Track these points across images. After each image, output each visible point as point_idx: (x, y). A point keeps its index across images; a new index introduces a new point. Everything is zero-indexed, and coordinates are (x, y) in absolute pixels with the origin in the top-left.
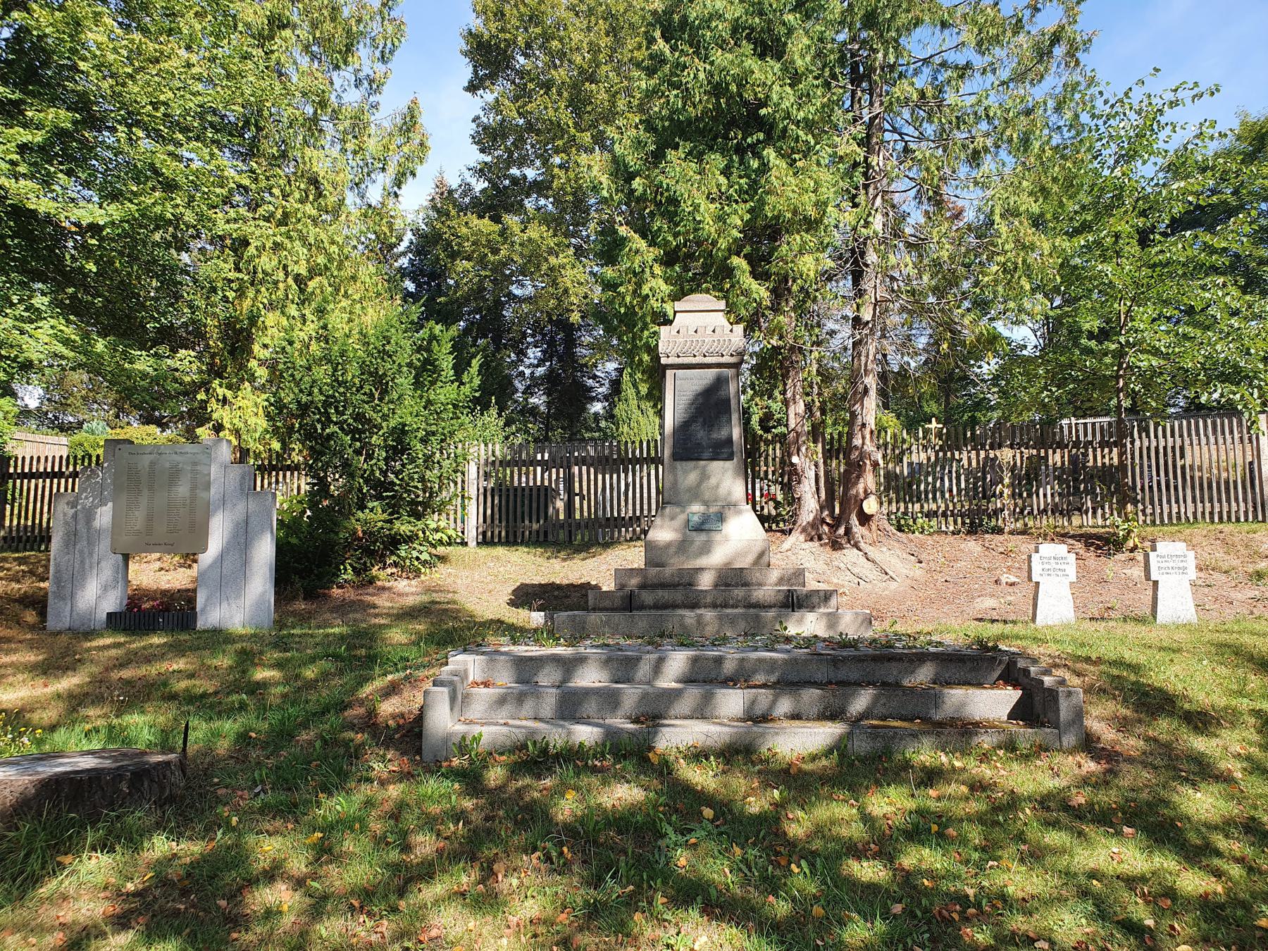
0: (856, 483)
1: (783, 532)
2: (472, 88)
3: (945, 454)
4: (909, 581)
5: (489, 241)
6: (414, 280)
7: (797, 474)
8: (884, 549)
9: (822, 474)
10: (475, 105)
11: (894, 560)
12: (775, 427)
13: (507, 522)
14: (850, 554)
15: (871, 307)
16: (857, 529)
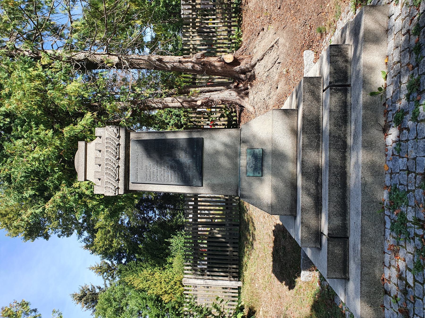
0: (214, 66)
1: (241, 111)
2: (47, 237)
3: (197, 26)
4: (279, 32)
5: (105, 234)
6: (122, 259)
7: (208, 102)
8: (255, 50)
9: (207, 89)
10: (53, 237)
11: (263, 44)
12: (181, 122)
13: (227, 264)
14: (259, 70)
15: (110, 56)
16: (243, 65)
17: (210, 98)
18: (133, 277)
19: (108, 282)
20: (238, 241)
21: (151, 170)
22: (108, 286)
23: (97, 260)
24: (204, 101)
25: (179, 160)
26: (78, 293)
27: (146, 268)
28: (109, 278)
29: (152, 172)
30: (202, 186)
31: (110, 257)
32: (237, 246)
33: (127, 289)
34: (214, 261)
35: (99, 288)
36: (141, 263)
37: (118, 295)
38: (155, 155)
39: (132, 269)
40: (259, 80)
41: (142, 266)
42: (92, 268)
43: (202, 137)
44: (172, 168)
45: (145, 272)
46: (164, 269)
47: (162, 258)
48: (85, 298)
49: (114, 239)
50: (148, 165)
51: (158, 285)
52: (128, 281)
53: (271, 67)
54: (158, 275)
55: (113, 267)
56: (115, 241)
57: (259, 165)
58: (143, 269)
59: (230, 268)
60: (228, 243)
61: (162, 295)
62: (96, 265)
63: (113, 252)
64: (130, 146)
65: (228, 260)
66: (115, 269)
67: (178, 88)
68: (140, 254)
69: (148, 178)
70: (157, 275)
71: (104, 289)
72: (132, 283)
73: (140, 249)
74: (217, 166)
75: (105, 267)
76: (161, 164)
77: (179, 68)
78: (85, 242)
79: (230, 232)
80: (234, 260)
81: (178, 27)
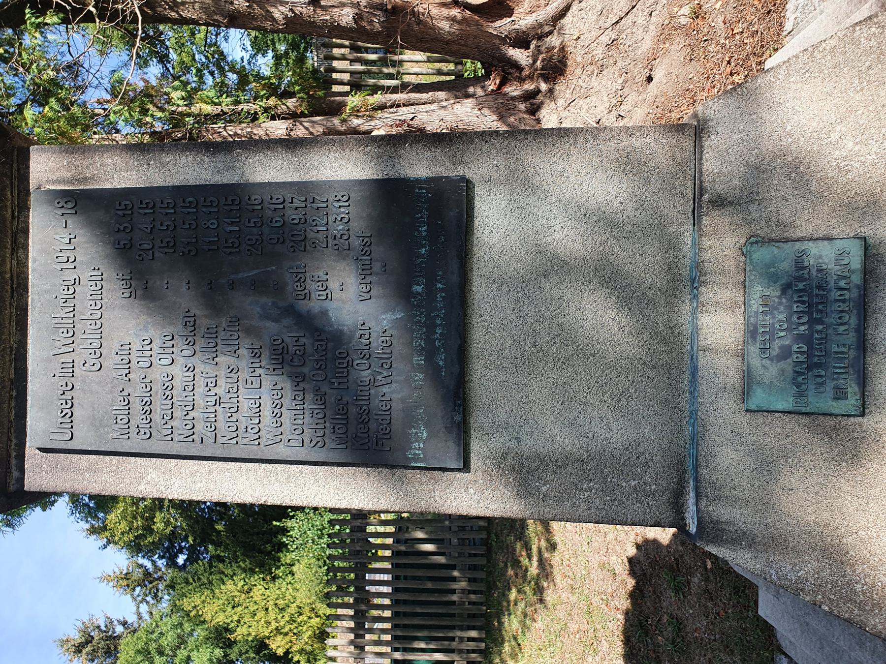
6: (176, 556)
13: (453, 628)
17: (415, 123)
18: (203, 598)
19: (144, 608)
20: (483, 561)
21: (157, 375)
22: (146, 616)
23: (119, 560)
24: (394, 131)
25: (324, 313)
26: (72, 637)
27: (232, 576)
28: (149, 599)
29: (158, 388)
30: (466, 467)
31: (149, 553)
32: (482, 575)
33: (187, 627)
34: (416, 621)
35: (124, 624)
36: (221, 565)
37: (168, 640)
38: (183, 294)
39: (199, 579)
40: (579, 59)
41: (223, 573)
42: (107, 579)
43: (460, 171)
44: (283, 360)
45: (230, 585)
46: (274, 579)
47: (269, 554)
48: (89, 648)
49: (158, 514)
50: (136, 345)
51: (260, 614)
52: (190, 608)
53: (626, 10)
54: (261, 592)
55: (156, 573)
56: (159, 517)
57: (843, 338)
58: (225, 579)
59: (461, 639)
60: (453, 567)
61: (269, 638)
62: (117, 570)
63: (154, 542)
64: (26, 232)
65: (453, 615)
66: (160, 578)
67: (307, 93)
68: (217, 545)
69: (138, 419)
70: (258, 592)
71: (136, 625)
72: (200, 613)
73: (219, 532)
74: (555, 349)
75: (138, 574)
76: (212, 334)
77: (312, 24)
78: (87, 521)
79: (461, 536)
80: (474, 616)
81: (305, 38)
